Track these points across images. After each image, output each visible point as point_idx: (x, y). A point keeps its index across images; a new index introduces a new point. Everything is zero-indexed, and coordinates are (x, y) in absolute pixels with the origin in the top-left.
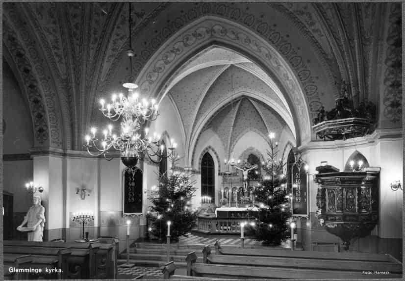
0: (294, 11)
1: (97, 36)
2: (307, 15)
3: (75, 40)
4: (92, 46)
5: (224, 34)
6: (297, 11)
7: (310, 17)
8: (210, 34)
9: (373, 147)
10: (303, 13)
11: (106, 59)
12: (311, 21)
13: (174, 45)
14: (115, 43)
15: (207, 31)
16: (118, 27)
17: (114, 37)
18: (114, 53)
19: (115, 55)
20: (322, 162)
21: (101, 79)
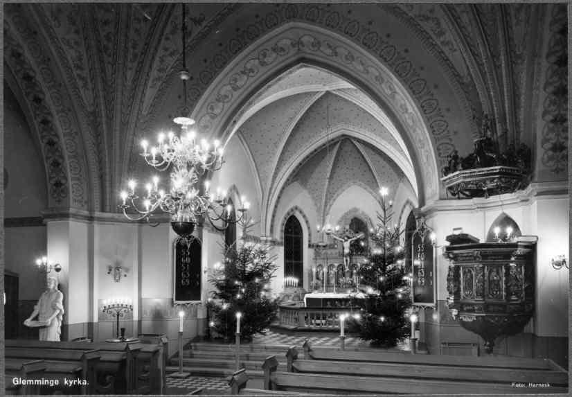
0: (415, 16)
1: (136, 51)
2: (433, 21)
3: (105, 56)
4: (130, 65)
5: (316, 48)
6: (420, 16)
7: (438, 24)
8: (297, 48)
9: (527, 207)
10: (427, 19)
11: (150, 83)
12: (439, 30)
13: (246, 64)
14: (162, 61)
15: (292, 44)
16: (167, 39)
17: (161, 52)
18: (161, 74)
19: (162, 77)
20: (454, 229)
21: (143, 112)
